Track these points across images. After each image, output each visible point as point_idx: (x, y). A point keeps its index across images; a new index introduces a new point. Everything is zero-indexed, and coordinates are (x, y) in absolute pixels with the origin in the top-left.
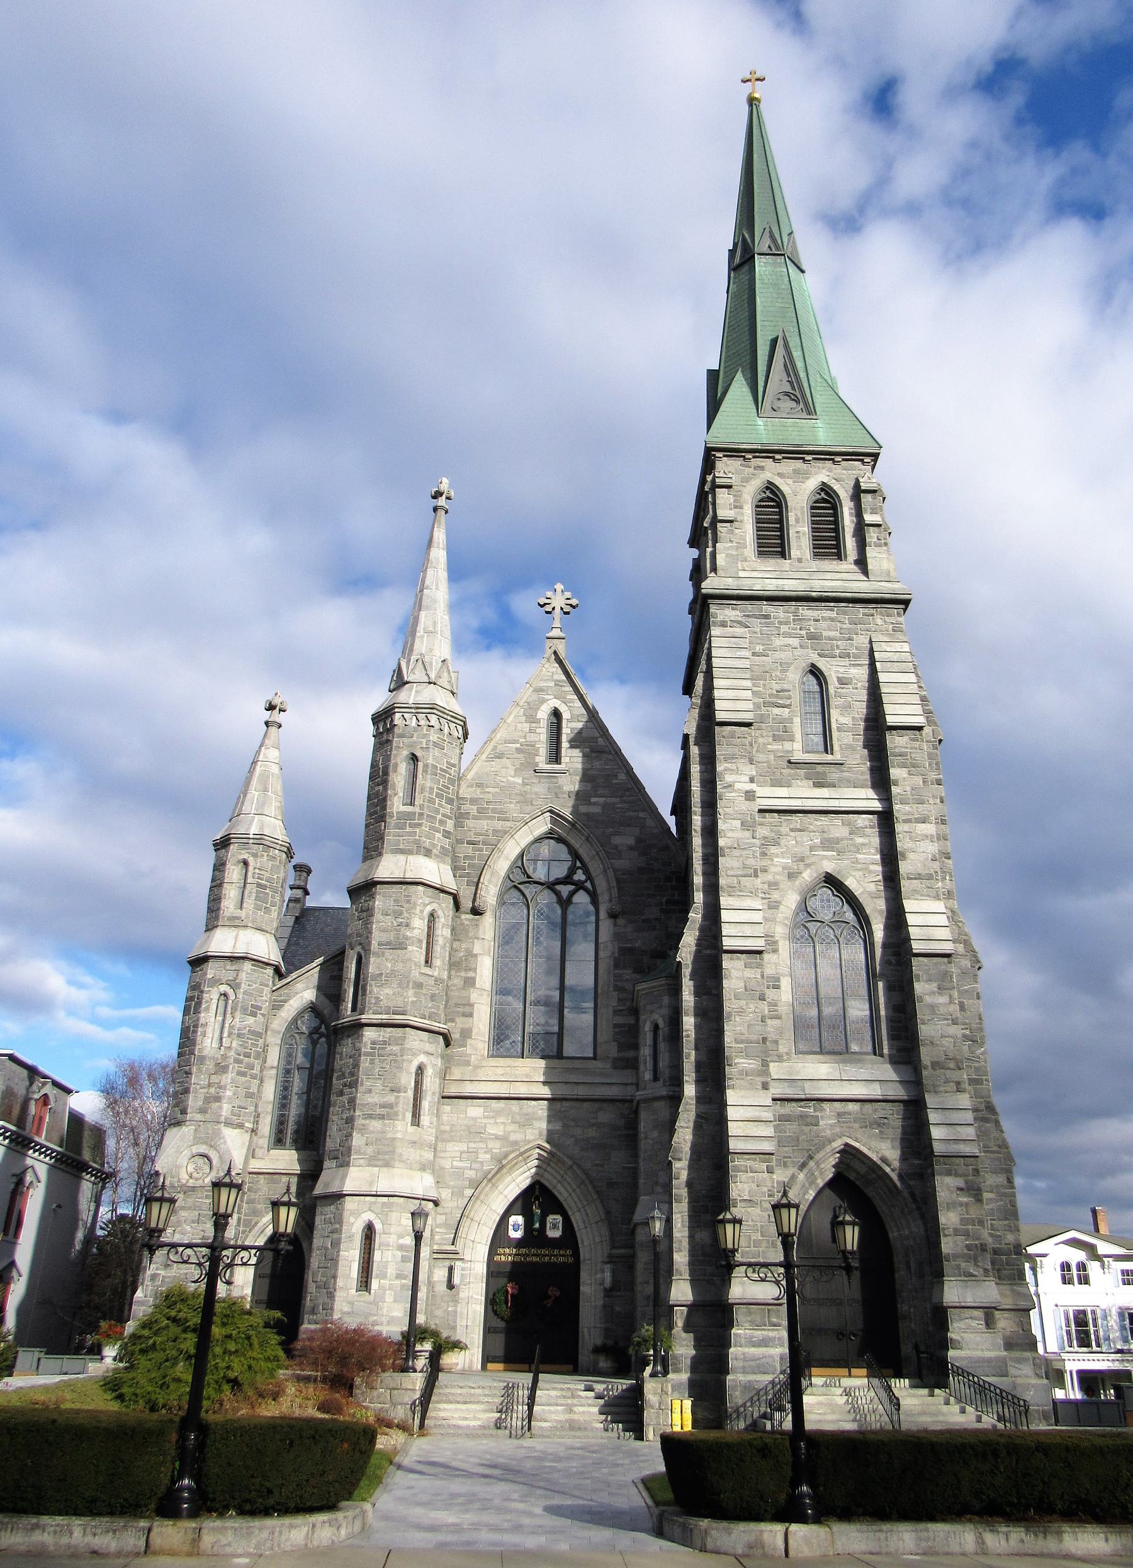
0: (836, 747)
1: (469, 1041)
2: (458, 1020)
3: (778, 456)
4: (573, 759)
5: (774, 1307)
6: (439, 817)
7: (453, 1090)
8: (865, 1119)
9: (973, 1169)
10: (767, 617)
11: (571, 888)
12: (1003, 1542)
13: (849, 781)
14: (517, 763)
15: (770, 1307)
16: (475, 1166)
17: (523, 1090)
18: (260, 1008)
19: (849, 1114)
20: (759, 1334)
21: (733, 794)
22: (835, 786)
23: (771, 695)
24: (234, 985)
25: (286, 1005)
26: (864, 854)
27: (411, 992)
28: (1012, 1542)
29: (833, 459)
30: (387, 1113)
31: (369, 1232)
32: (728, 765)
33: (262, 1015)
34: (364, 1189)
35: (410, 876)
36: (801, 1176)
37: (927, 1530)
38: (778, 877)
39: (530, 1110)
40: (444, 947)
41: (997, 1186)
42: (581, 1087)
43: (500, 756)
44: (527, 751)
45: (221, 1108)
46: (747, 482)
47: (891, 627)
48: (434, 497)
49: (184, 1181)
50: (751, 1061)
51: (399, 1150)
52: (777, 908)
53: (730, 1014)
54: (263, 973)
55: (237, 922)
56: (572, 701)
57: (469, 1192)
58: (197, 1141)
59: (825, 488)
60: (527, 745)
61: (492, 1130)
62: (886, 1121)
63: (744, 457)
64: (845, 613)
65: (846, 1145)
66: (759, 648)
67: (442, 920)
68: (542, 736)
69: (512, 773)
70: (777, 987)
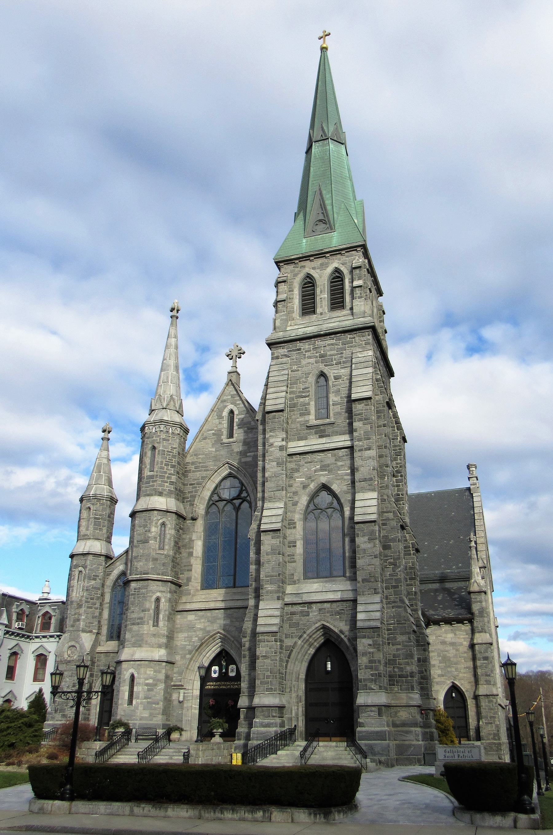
0: (331, 415)
1: (190, 583)
2: (185, 573)
3: (311, 258)
4: (239, 434)
5: (275, 708)
7: (180, 608)
8: (332, 611)
9: (378, 634)
10: (299, 349)
11: (240, 501)
12: (141, 811)
13: (337, 432)
15: (273, 708)
17: (212, 605)
18: (98, 576)
19: (325, 609)
21: (273, 449)
23: (299, 392)
24: (85, 567)
26: (342, 471)
27: (151, 563)
28: (145, 811)
29: (341, 253)
30: (140, 622)
31: (132, 677)
33: (99, 579)
35: (150, 507)
36: (300, 642)
37: (111, 805)
38: (298, 489)
39: (215, 615)
40: (170, 539)
41: (403, 642)
42: (239, 601)
43: (205, 439)
44: (218, 434)
45: (80, 624)
46: (296, 276)
47: (364, 343)
48: (171, 311)
50: (273, 586)
53: (263, 563)
54: (98, 559)
55: (86, 537)
56: (239, 404)
57: (188, 656)
58: (71, 640)
59: (337, 270)
60: (218, 431)
61: (198, 626)
62: (343, 611)
63: (294, 262)
65: (323, 625)
66: (295, 367)
67: (169, 526)
68: (225, 424)
69: (211, 446)
70: (295, 546)
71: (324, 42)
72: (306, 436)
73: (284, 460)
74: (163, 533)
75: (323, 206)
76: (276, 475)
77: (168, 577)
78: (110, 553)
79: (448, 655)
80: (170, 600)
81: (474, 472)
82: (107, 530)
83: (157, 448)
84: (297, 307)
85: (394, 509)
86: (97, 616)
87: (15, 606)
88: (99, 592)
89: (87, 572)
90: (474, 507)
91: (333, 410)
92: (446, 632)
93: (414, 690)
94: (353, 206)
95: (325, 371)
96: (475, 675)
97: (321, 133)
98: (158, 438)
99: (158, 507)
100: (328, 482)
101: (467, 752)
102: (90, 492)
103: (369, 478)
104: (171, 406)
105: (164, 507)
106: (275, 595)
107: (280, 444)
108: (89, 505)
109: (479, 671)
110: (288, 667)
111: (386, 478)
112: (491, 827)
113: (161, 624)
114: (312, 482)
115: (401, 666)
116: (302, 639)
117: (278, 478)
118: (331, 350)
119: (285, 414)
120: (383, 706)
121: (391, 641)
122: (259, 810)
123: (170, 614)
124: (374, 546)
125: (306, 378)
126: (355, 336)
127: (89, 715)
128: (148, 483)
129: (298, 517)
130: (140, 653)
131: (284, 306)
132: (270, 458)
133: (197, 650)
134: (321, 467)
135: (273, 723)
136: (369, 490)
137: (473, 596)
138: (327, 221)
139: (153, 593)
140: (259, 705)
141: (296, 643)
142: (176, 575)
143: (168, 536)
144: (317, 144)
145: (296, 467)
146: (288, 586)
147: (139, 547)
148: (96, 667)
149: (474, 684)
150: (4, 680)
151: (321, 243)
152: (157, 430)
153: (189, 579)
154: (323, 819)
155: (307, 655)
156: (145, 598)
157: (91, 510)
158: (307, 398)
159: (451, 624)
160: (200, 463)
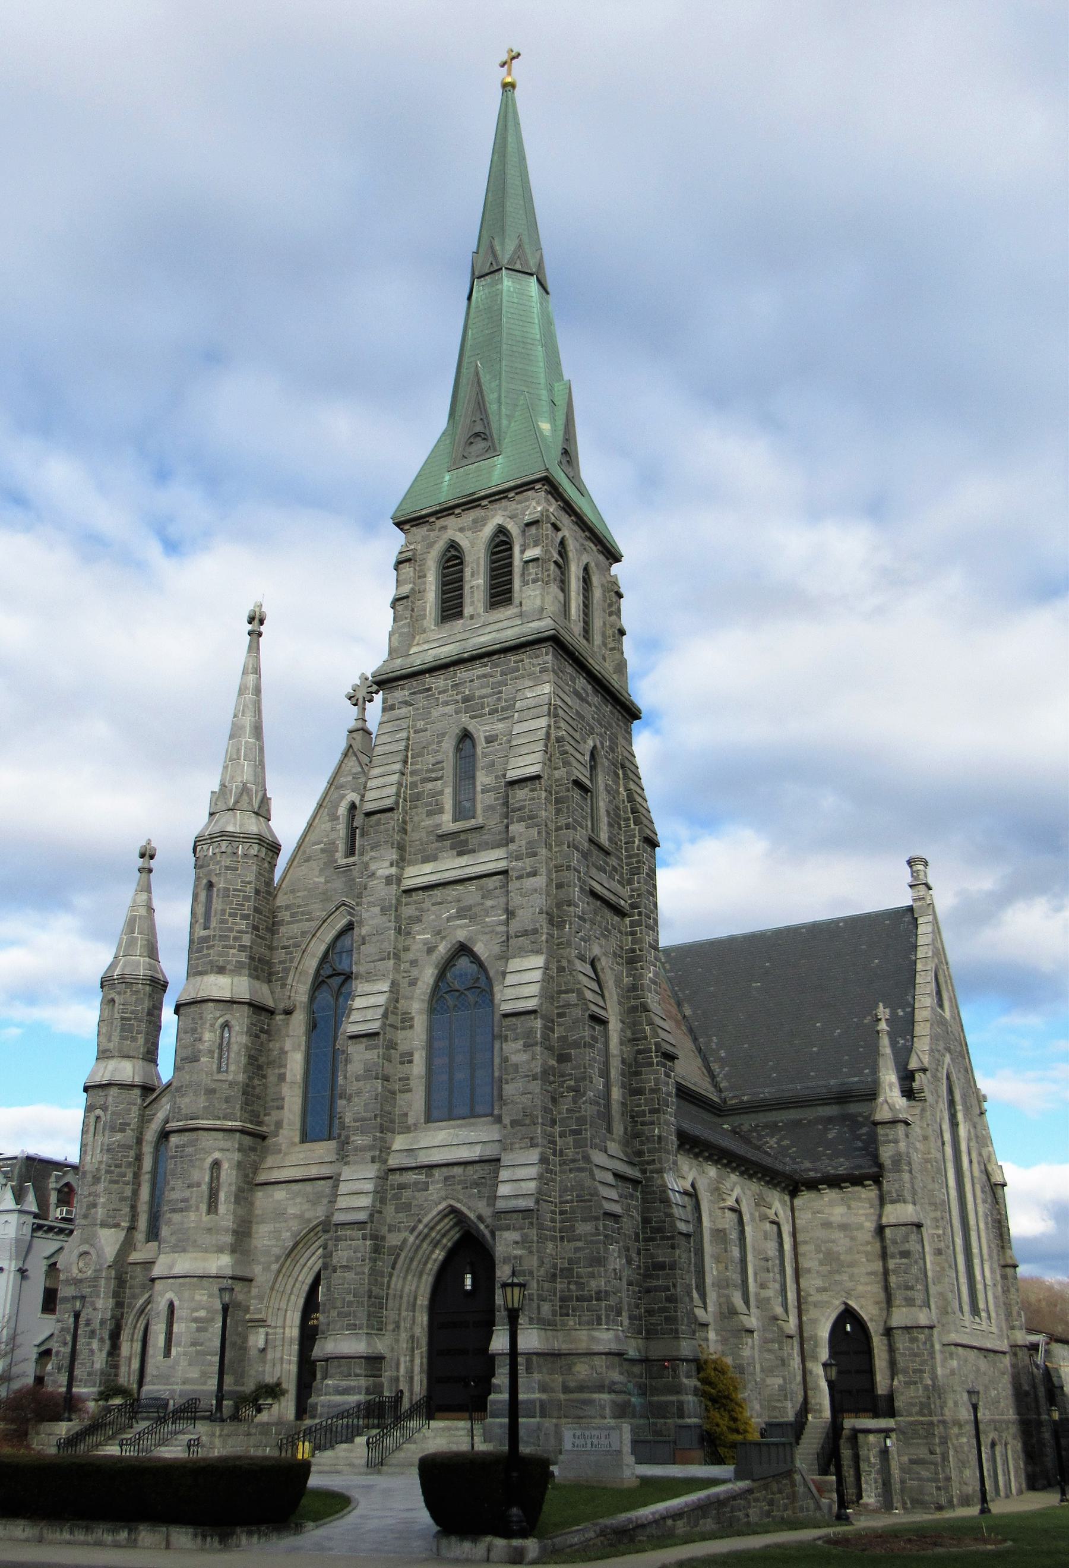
1: (281, 1131)
3: (457, 511)
7: (262, 1177)
8: (466, 1180)
10: (429, 689)
13: (487, 843)
17: (314, 1171)
18: (129, 1125)
19: (454, 1177)
21: (375, 882)
22: (474, 852)
23: (429, 771)
25: (155, 1118)
27: (203, 1098)
29: (506, 497)
31: (171, 1306)
32: (373, 854)
35: (201, 995)
38: (419, 954)
40: (239, 1053)
43: (307, 860)
44: (329, 850)
45: (96, 1213)
47: (538, 669)
49: (74, 1275)
54: (129, 1094)
59: (501, 530)
62: (483, 1180)
64: (497, 666)
65: (451, 1206)
66: (420, 724)
67: (237, 1028)
70: (411, 1062)
71: (509, 73)
73: (394, 902)
76: (379, 932)
77: (234, 1123)
78: (153, 1080)
79: (836, 1249)
80: (239, 1165)
81: (922, 873)
82: (146, 1039)
83: (215, 885)
84: (430, 607)
85: (578, 986)
86: (128, 1197)
87: (53, 1179)
88: (132, 1153)
92: (831, 1204)
93: (601, 1325)
95: (471, 728)
96: (887, 1288)
97: (491, 259)
99: (216, 994)
101: (603, 1436)
102: (114, 971)
103: (533, 929)
104: (244, 803)
105: (226, 995)
106: (368, 1155)
109: (893, 1279)
110: (392, 1286)
111: (567, 926)
112: (457, 1561)
113: (222, 1208)
114: (442, 941)
115: (582, 1280)
116: (415, 1233)
117: (382, 937)
118: (482, 688)
120: (534, 1354)
121: (567, 1234)
122: (123, 1528)
123: (240, 1190)
124: (533, 1059)
129: (417, 1006)
130: (183, 1264)
132: (371, 899)
133: (288, 1255)
134: (457, 912)
135: (355, 1386)
136: (532, 951)
137: (880, 1130)
138: (488, 434)
139: (207, 1152)
140: (334, 1356)
141: (405, 1241)
143: (235, 1048)
144: (483, 282)
145: (417, 913)
146: (397, 1136)
147: (184, 1069)
148: (127, 1290)
149: (884, 1305)
150: (39, 1315)
151: (474, 480)
153: (279, 1125)
154: (216, 1544)
155: (431, 1262)
157: (117, 1005)
160: (299, 907)
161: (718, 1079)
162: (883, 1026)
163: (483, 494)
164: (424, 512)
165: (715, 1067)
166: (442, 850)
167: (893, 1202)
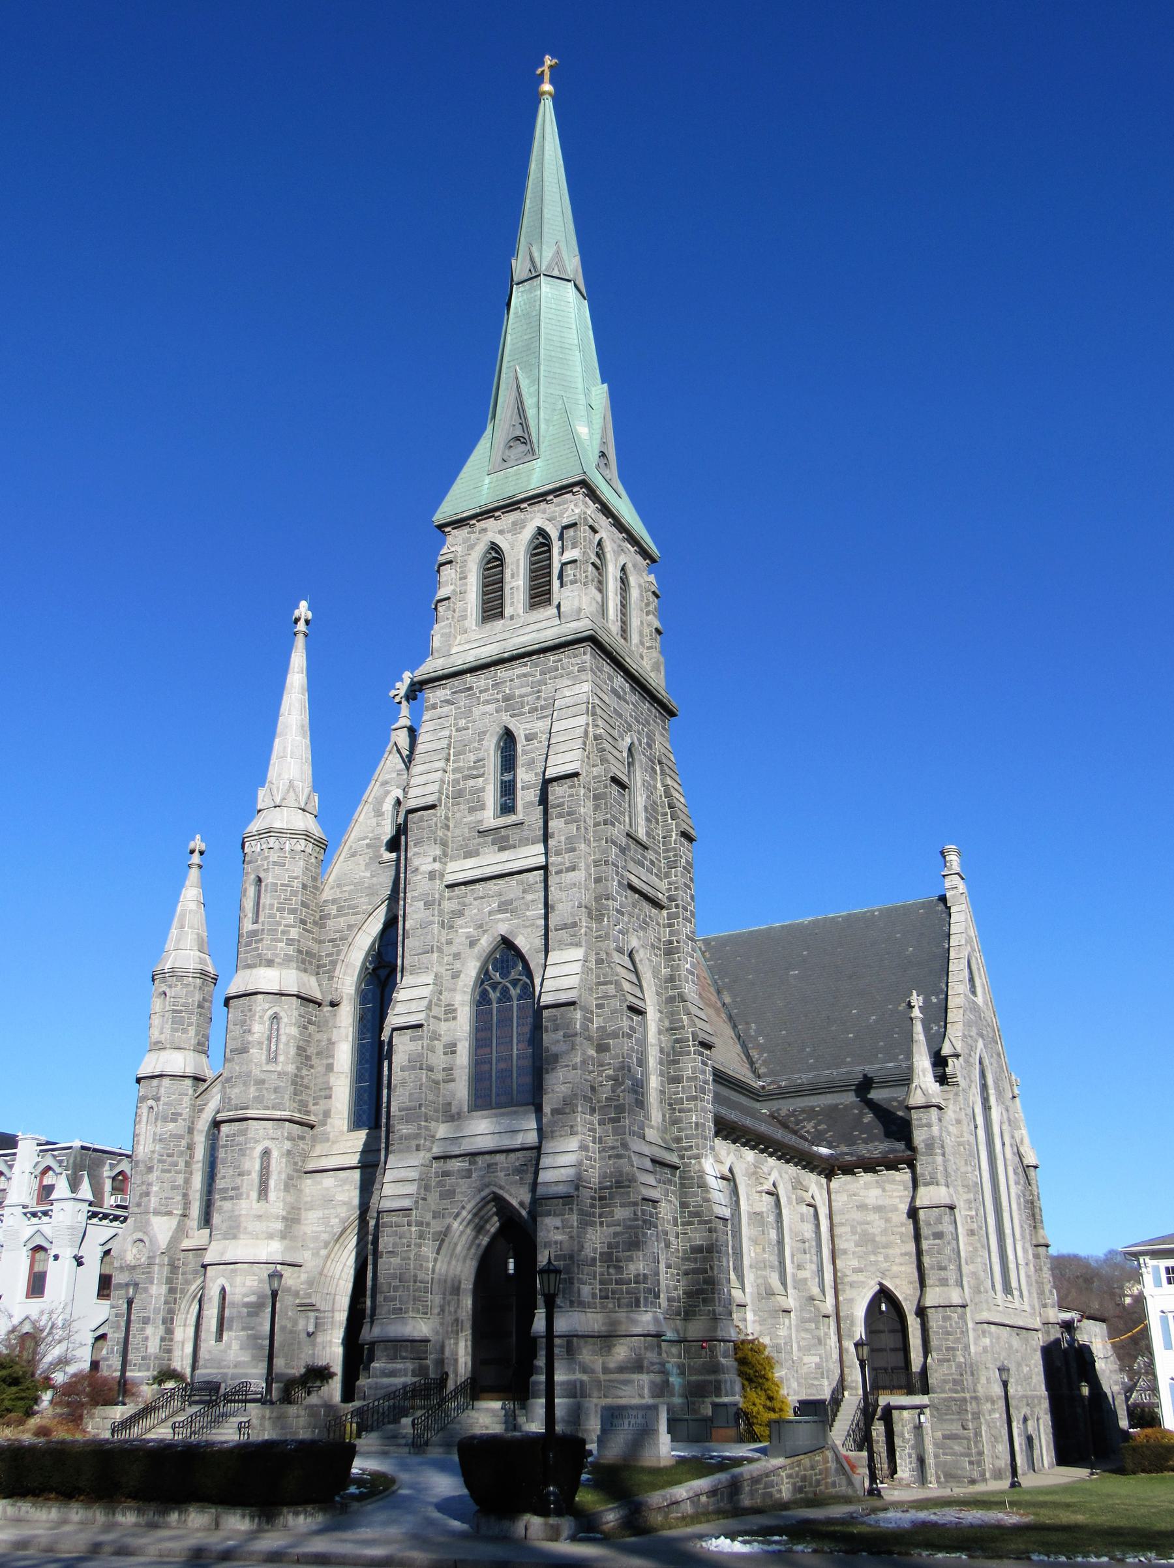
1: (329, 1120)
3: (497, 514)
6: (280, 929)
7: (311, 1166)
10: (470, 689)
13: (527, 839)
14: (367, 857)
16: (328, 1229)
18: (181, 1115)
20: (391, 1366)
23: (470, 768)
24: (157, 1099)
34: (217, 1260)
35: (250, 988)
40: (287, 1044)
47: (576, 668)
51: (243, 1225)
52: (458, 977)
55: (160, 1046)
57: (324, 1252)
59: (541, 532)
62: (525, 1168)
64: (537, 665)
65: (494, 1193)
66: (462, 723)
69: (363, 868)
72: (478, 849)
73: (437, 896)
74: (274, 1035)
75: (521, 411)
76: (425, 925)
77: (283, 1113)
79: (871, 1230)
86: (179, 1186)
87: (107, 1167)
88: (184, 1143)
89: (161, 1108)
90: (949, 935)
91: (522, 799)
92: (867, 1186)
94: (581, 402)
98: (265, 862)
100: (511, 933)
105: (275, 988)
107: (429, 868)
108: (164, 988)
109: (926, 1260)
111: (606, 920)
113: (272, 1195)
116: (459, 1220)
119: (441, 811)
122: (173, 1509)
123: (290, 1178)
125: (480, 741)
126: (562, 656)
127: (170, 1360)
128: (249, 944)
131: (448, 608)
136: (571, 944)
137: (915, 1115)
138: (527, 438)
141: (449, 1227)
142: (303, 1107)
144: (521, 288)
152: (264, 846)
153: (327, 1114)
156: (243, 1153)
158: (481, 779)
159: (875, 1172)
161: (757, 1065)
162: (916, 1013)
163: (522, 496)
164: (465, 515)
165: (754, 1054)
166: (483, 845)
167: (926, 1184)
